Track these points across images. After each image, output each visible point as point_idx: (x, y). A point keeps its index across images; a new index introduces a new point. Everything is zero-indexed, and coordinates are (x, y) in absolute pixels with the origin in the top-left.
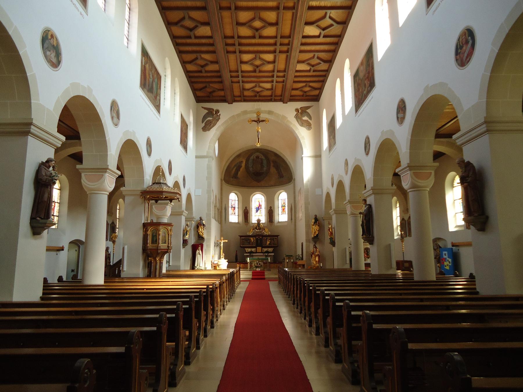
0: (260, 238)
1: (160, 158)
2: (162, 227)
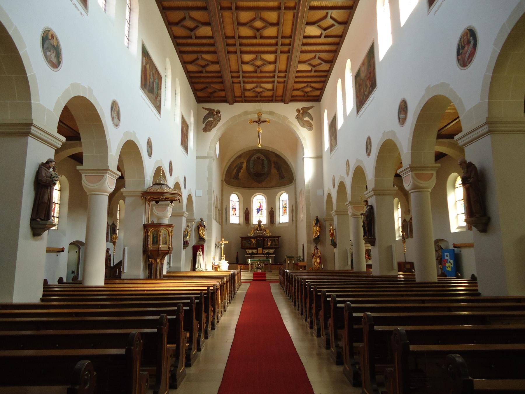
0: (261, 239)
1: (161, 159)
2: (162, 228)
